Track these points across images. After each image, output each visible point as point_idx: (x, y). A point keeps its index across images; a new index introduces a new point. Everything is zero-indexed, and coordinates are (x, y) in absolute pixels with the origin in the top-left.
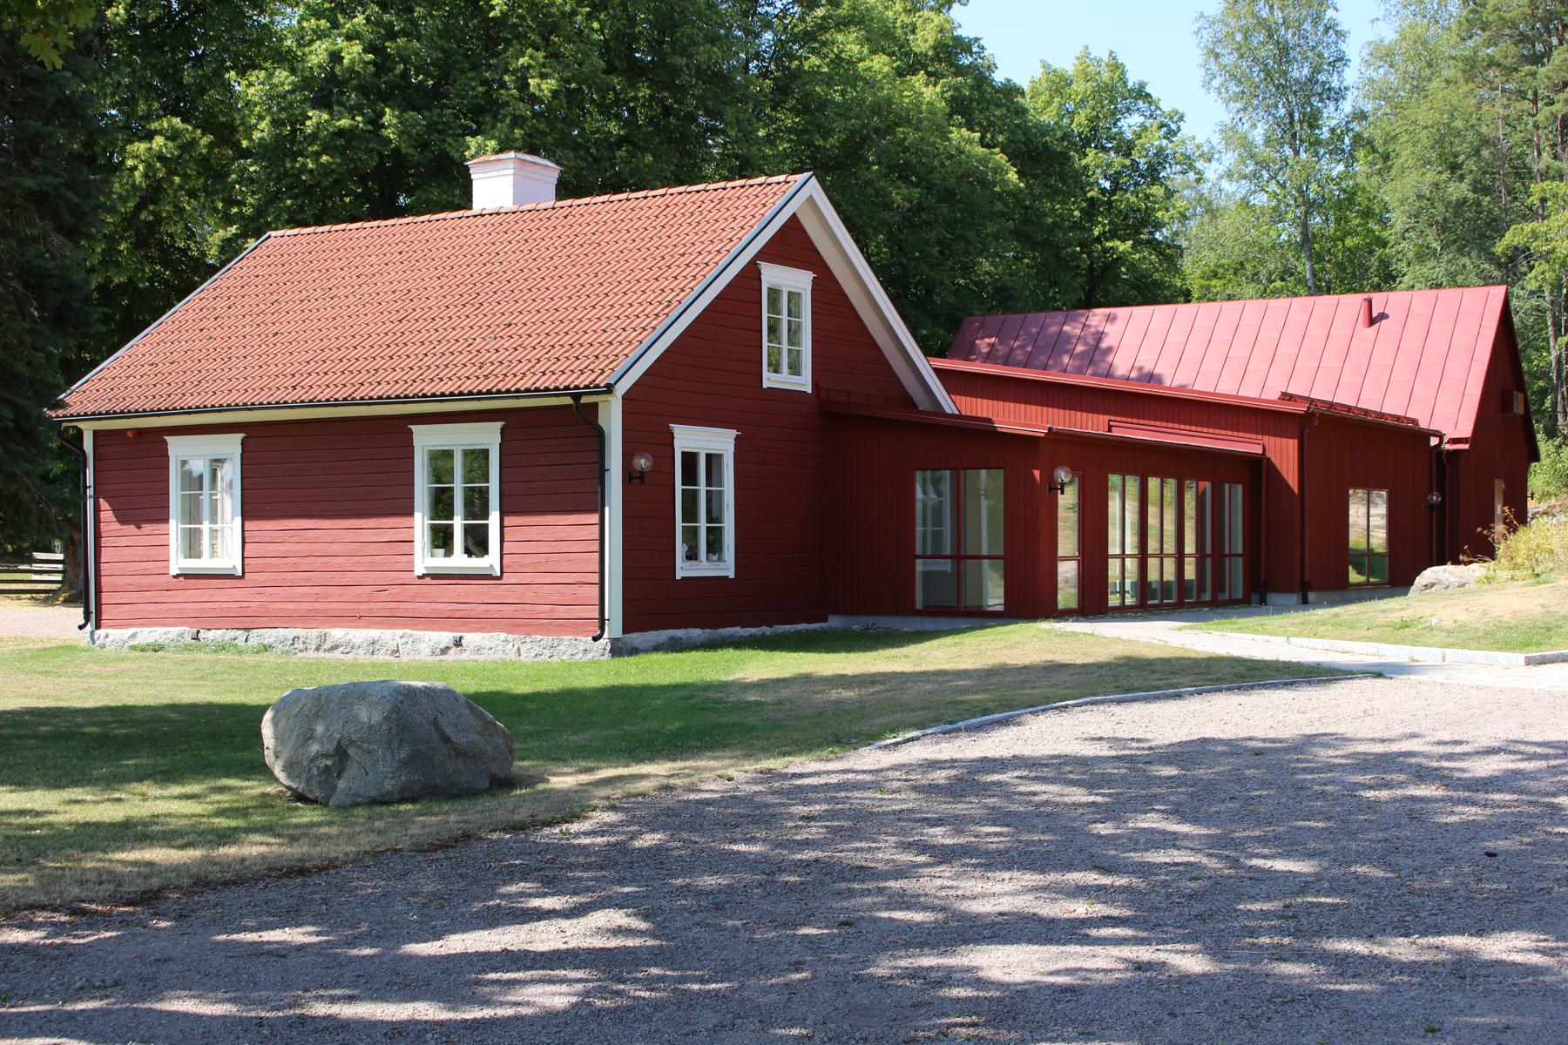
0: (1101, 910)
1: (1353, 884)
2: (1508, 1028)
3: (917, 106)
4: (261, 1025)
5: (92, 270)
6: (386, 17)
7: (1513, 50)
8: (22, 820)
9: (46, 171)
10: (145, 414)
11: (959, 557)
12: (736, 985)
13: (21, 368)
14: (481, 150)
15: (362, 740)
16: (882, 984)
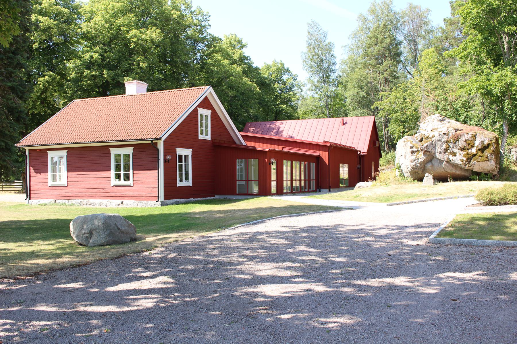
0: (294, 273)
1: (357, 264)
2: (408, 305)
3: (235, 72)
4: (65, 314)
5: (29, 110)
6: (104, 47)
7: (375, 62)
8: (5, 251)
9: (14, 81)
10: (42, 145)
11: (247, 181)
12: (199, 298)
13: (7, 132)
14: (128, 80)
15: (96, 229)
16: (239, 297)
